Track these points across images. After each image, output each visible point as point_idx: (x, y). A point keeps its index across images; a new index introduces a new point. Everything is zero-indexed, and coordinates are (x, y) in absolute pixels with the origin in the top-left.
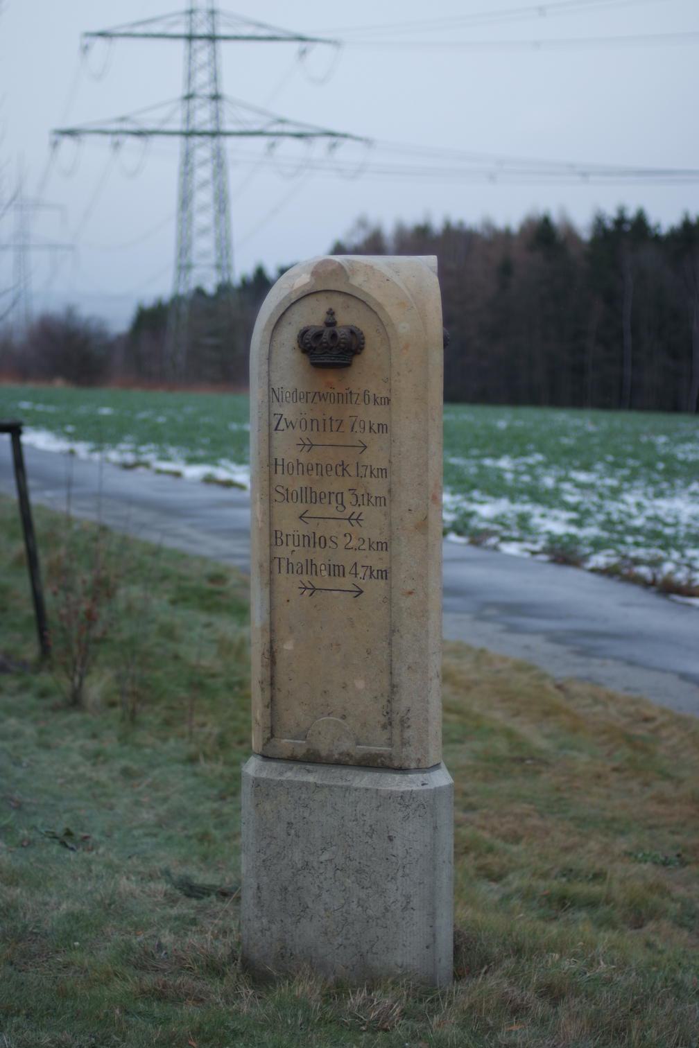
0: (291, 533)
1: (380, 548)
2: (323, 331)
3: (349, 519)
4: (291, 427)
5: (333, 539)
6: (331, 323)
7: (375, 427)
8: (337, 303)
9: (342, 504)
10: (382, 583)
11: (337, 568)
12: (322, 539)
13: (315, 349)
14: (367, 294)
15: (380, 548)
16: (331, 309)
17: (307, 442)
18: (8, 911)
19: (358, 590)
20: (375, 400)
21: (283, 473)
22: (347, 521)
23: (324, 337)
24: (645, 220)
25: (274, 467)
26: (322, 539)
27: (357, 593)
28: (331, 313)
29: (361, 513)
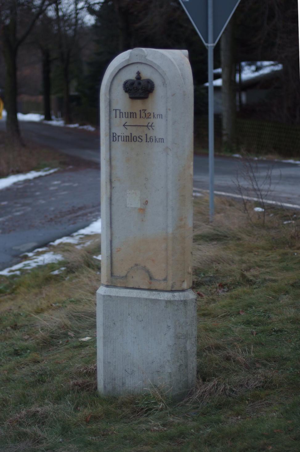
0: (121, 135)
2: (135, 82)
5: (140, 137)
7: (158, 140)
8: (140, 68)
13: (131, 90)
14: (152, 62)
17: (150, 128)
19: (125, 126)
22: (146, 127)
23: (135, 84)
24: (152, 81)
28: (139, 73)
29: (126, 122)
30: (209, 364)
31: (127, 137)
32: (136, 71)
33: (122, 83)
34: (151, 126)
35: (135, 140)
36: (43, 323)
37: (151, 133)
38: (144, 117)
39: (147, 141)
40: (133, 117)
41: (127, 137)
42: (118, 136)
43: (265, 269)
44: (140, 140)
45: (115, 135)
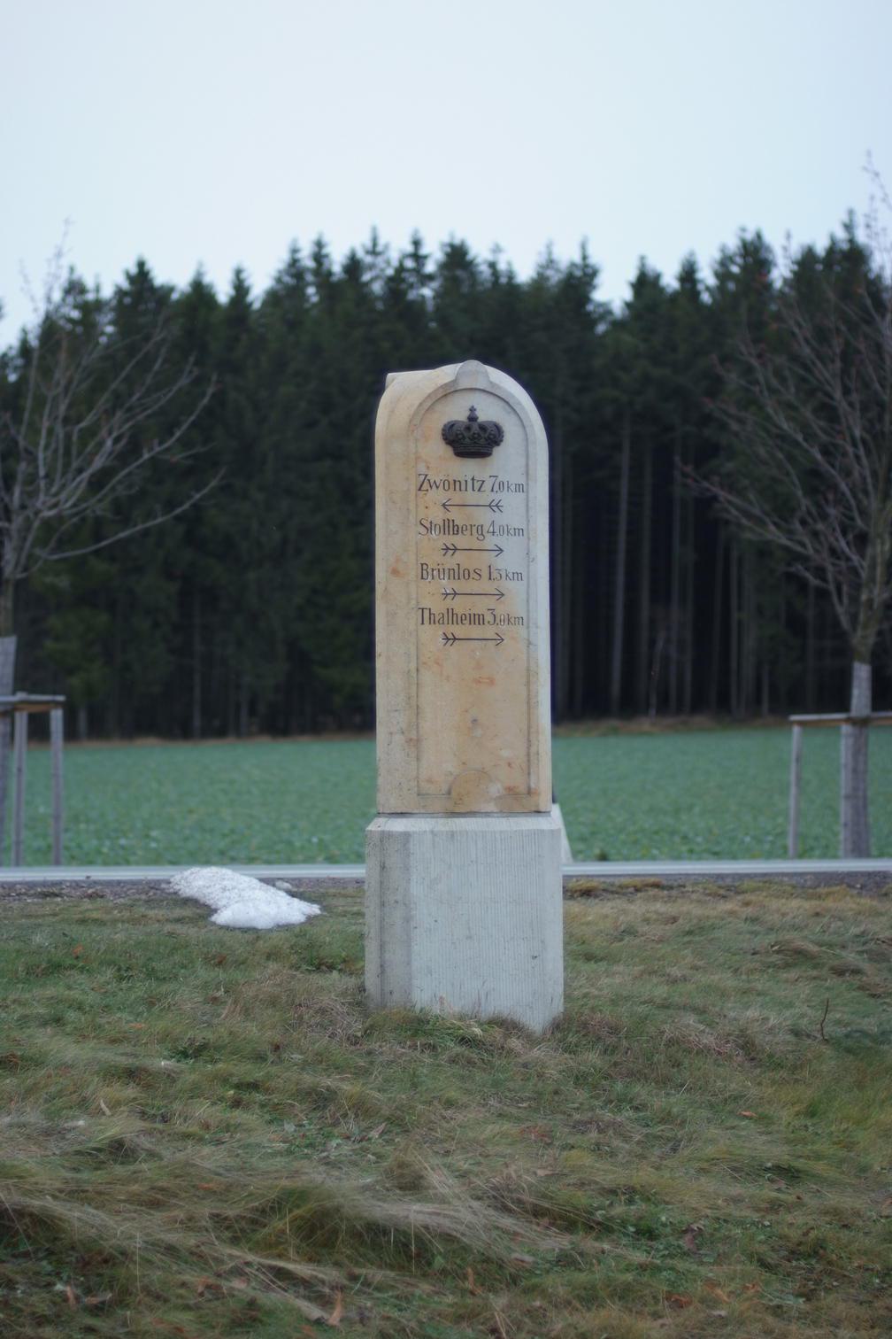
1: (516, 578)
3: (490, 506)
4: (434, 487)
6: (472, 418)
7: (513, 487)
9: (482, 534)
10: (522, 496)
11: (477, 617)
12: (466, 572)
15: (516, 578)
16: (473, 407)
17: (495, 508)
18: (57, 955)
20: (508, 532)
21: (423, 623)
25: (414, 687)
26: (466, 572)
27: (498, 597)
28: (472, 410)
30: (321, 297)
31: (452, 572)
32: (469, 405)
33: (440, 426)
34: (497, 506)
35: (467, 577)
36: (822, 423)
37: (501, 610)
38: (492, 622)
39: (490, 579)
40: (479, 624)
41: (452, 572)
42: (433, 570)
43: (123, 916)
44: (477, 577)
45: (425, 567)
